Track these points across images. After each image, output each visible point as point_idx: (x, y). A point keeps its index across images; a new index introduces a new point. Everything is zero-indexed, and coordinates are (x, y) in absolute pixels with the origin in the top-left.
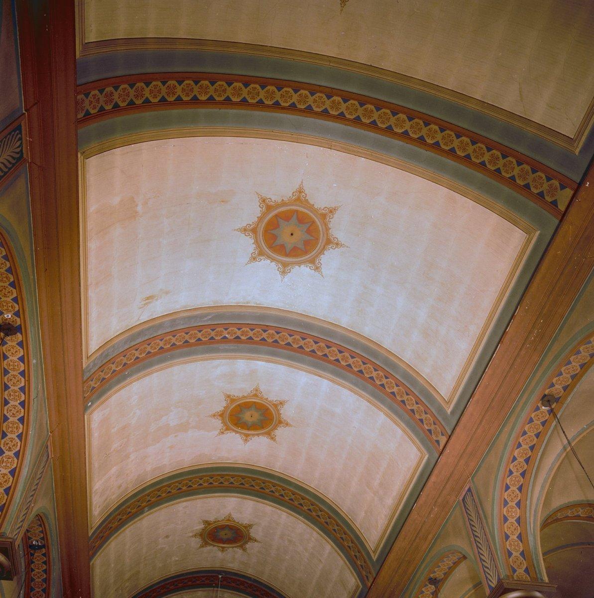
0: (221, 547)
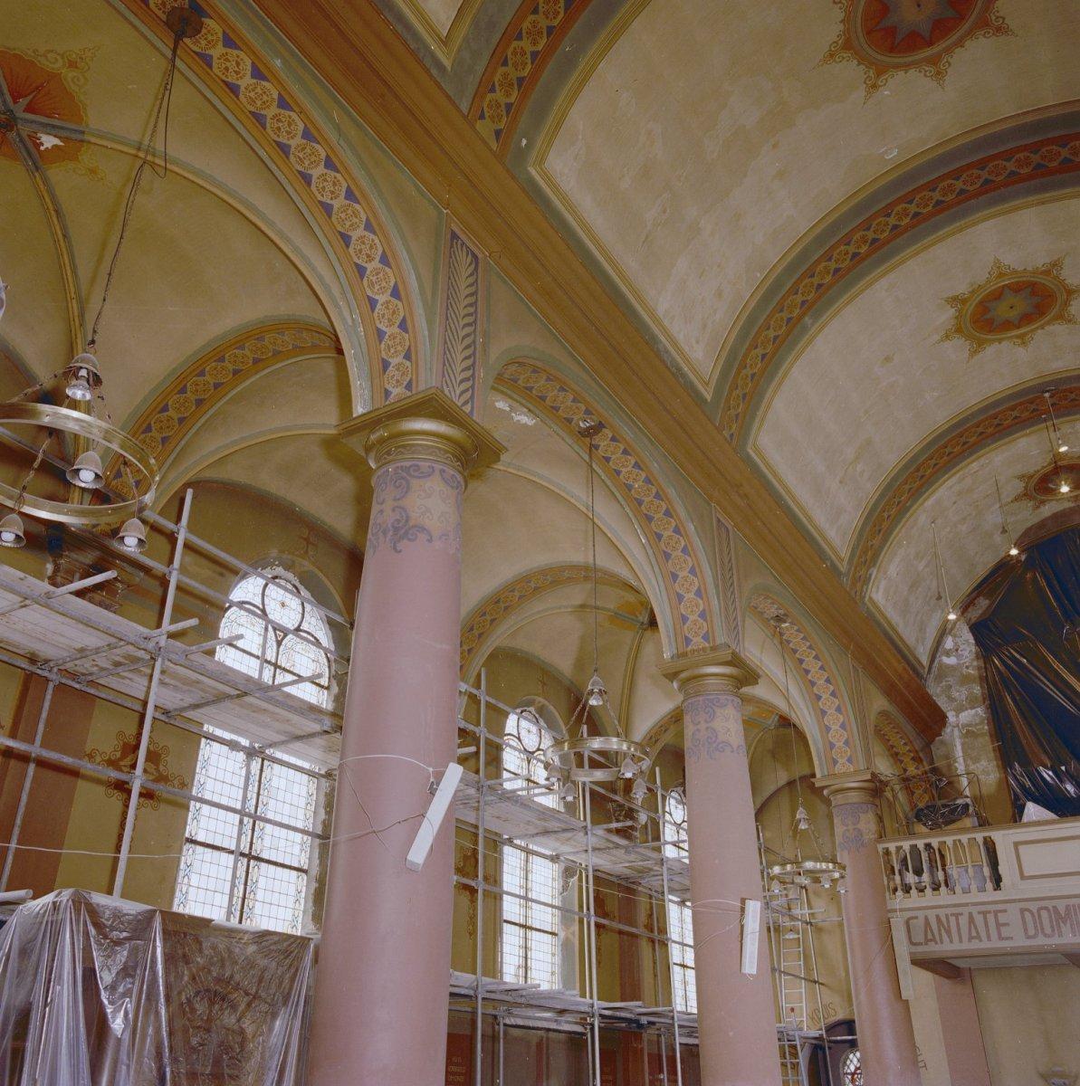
0: (1017, 337)
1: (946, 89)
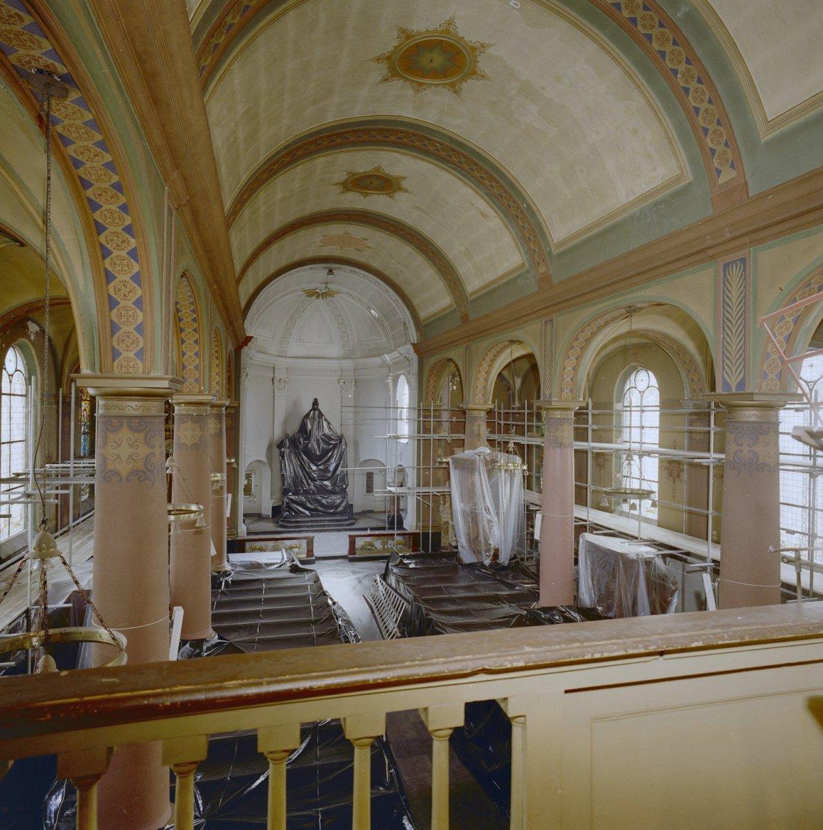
1: (453, 13)
